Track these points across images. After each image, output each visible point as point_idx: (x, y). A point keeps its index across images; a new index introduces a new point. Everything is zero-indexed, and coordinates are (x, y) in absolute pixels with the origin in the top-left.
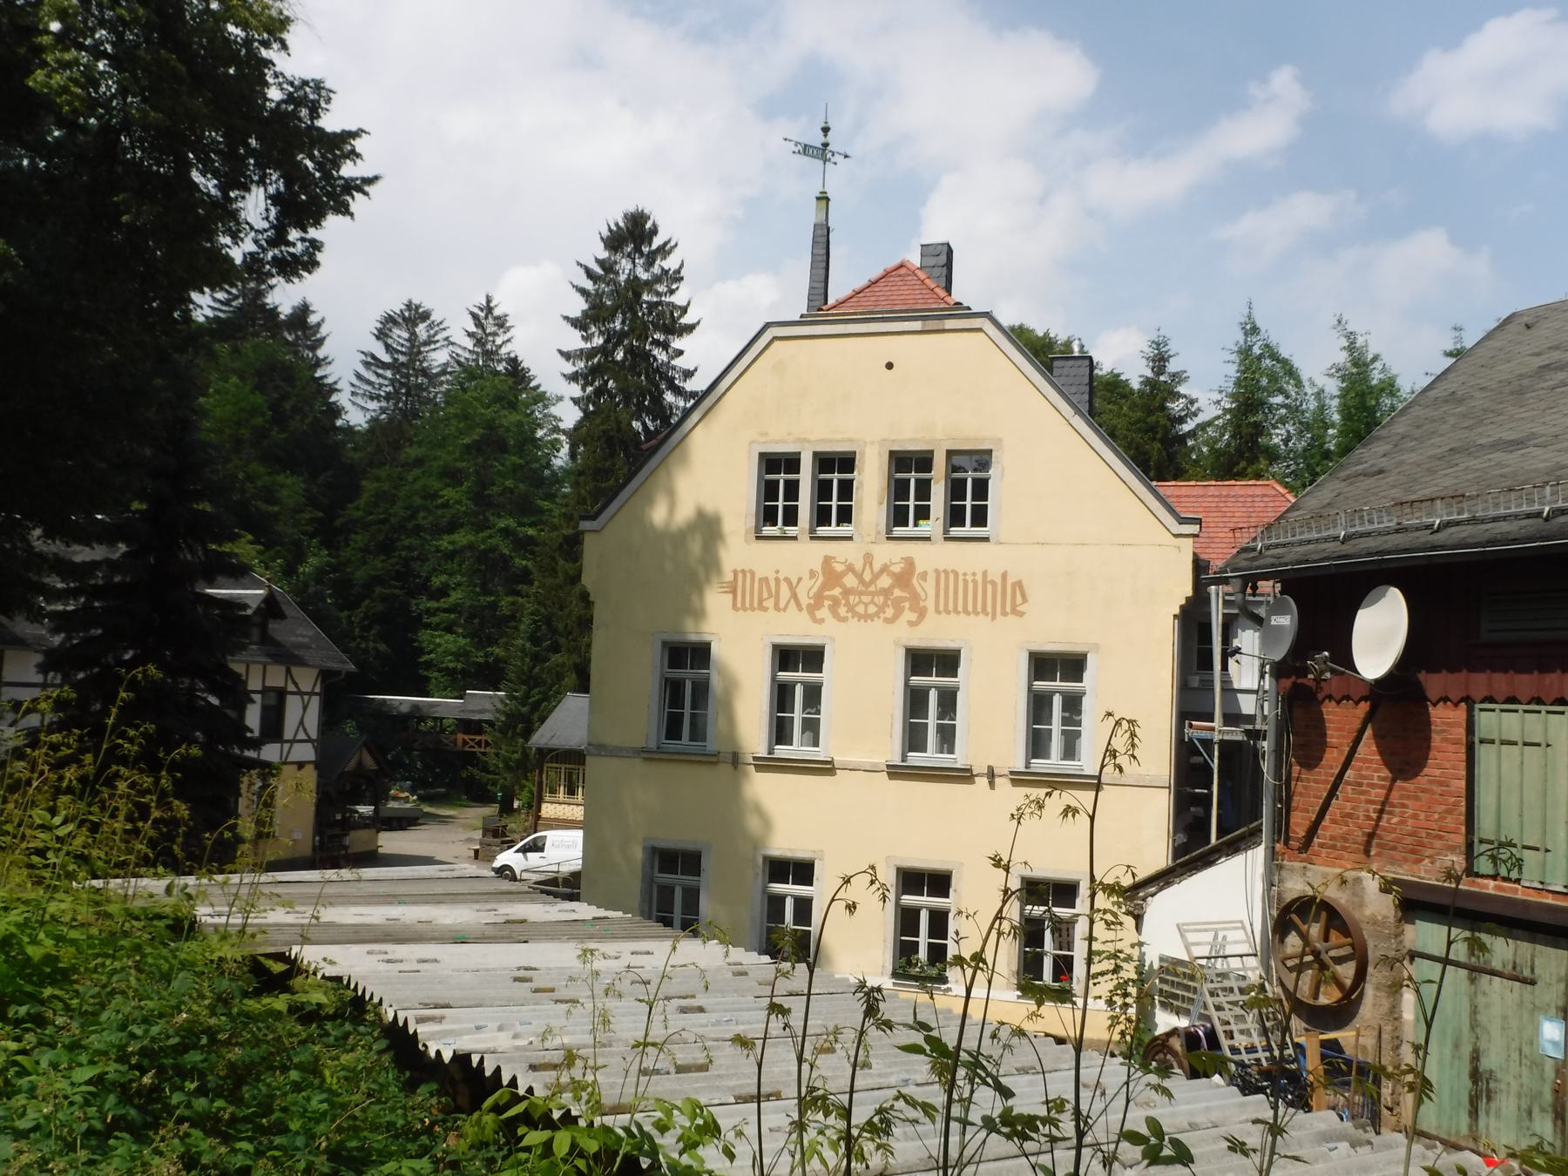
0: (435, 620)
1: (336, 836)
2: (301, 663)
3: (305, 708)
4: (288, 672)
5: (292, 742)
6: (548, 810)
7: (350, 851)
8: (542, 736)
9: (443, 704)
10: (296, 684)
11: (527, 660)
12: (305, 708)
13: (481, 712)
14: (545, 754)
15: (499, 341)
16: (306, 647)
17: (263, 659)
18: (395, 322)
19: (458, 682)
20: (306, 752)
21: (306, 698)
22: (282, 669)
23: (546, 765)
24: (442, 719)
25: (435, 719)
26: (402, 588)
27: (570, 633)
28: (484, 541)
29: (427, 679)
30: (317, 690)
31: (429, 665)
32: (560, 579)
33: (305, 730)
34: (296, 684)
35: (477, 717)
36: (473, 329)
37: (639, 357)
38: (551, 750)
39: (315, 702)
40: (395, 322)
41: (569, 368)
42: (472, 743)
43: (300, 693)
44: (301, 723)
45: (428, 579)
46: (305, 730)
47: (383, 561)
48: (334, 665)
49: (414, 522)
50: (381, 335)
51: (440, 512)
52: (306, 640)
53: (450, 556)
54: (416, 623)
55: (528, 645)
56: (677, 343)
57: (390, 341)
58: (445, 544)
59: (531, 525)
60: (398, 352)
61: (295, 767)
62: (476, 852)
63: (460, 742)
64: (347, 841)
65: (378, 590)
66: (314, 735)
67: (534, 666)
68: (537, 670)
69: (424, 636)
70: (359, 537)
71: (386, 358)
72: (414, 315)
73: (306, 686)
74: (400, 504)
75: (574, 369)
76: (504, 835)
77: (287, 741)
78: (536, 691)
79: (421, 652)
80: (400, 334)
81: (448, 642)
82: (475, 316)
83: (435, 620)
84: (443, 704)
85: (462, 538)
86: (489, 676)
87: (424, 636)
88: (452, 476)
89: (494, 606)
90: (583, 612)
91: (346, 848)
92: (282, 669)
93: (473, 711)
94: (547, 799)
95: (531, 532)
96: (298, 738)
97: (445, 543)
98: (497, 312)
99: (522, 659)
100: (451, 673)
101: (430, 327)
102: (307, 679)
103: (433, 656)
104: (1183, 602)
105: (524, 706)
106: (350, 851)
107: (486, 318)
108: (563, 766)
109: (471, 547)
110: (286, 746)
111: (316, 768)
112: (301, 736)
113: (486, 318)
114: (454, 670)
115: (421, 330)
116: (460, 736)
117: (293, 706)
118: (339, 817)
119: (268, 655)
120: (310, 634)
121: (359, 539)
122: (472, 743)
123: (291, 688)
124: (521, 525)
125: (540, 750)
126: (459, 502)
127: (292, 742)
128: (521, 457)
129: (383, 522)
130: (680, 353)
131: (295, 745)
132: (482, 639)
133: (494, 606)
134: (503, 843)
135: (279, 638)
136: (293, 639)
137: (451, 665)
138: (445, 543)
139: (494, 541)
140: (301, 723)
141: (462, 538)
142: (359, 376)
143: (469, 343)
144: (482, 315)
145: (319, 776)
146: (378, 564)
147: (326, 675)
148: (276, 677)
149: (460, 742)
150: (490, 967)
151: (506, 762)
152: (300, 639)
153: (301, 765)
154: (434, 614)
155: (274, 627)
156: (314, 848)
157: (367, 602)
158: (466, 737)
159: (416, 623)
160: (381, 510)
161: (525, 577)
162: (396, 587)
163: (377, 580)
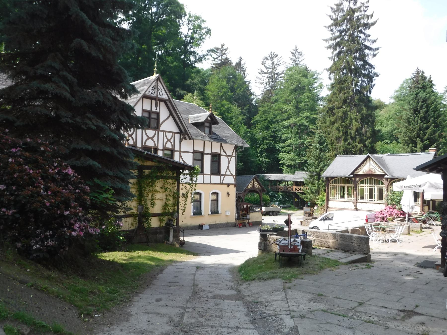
0: (284, 150)
1: (245, 214)
2: (226, 142)
3: (229, 162)
4: (221, 146)
5: (225, 175)
6: (331, 204)
7: (250, 221)
8: (328, 172)
9: (289, 177)
10: (225, 152)
11: (318, 151)
12: (229, 162)
13: (301, 178)
14: (329, 180)
15: (300, 60)
16: (229, 137)
17: (210, 140)
18: (267, 59)
19: (293, 168)
20: (231, 180)
21: (229, 158)
22: (219, 144)
23: (330, 185)
24: (288, 181)
25: (286, 181)
26: (273, 140)
27: (333, 143)
28: (299, 121)
29: (282, 169)
30: (234, 155)
31: (282, 164)
32: (328, 124)
33: (230, 171)
34: (225, 152)
35: (299, 180)
36: (292, 57)
37: (354, 39)
38: (332, 178)
39: (233, 160)
40: (267, 59)
41: (327, 44)
42: (298, 189)
43: (226, 155)
44: (228, 168)
45: (281, 137)
46: (230, 171)
47: (266, 132)
48: (240, 144)
49: (276, 119)
50: (263, 63)
51: (284, 114)
52: (229, 135)
53: (287, 127)
54: (278, 151)
55: (318, 145)
56: (368, 32)
57: (266, 65)
58: (286, 123)
59: (315, 114)
60: (268, 68)
61: (226, 186)
62: (302, 222)
63: (294, 189)
64: (249, 216)
65: (265, 141)
66: (234, 173)
67: (321, 153)
68: (322, 154)
69: (281, 155)
70: (259, 126)
71: (266, 71)
72: (273, 56)
73: (229, 153)
74: (271, 114)
75: (329, 45)
76: (313, 215)
77: (222, 175)
78: (322, 162)
79: (280, 160)
80: (268, 63)
81: (288, 156)
82: (292, 53)
83: (284, 150)
84: (289, 177)
85: (292, 121)
86: (301, 167)
87: (281, 155)
88: (287, 102)
89: (303, 143)
90: (337, 135)
91: (249, 219)
92: (219, 144)
93: (298, 178)
94: (331, 199)
95: (315, 116)
96: (227, 174)
97: (286, 123)
98: (299, 51)
99: (316, 151)
100: (289, 166)
101: (278, 59)
102: (229, 149)
103: (284, 161)
104: (251, 257)
105: (317, 169)
106: (250, 221)
107: (296, 53)
108: (338, 185)
109: (295, 124)
110: (222, 177)
111: (235, 187)
112: (228, 173)
113: (296, 53)
114: (291, 165)
115: (276, 61)
116: (294, 187)
117: (224, 161)
118: (245, 206)
119: (211, 138)
120: (231, 133)
121: (259, 126)
122: (298, 189)
123: (223, 153)
124: (312, 114)
125: (327, 178)
126: (290, 109)
127: (225, 175)
128: (310, 93)
129: (266, 120)
130: (369, 36)
131: (226, 177)
132: (299, 155)
133: (303, 143)
134: (312, 218)
135: (217, 133)
136: (223, 134)
137: (289, 164)
138: (286, 123)
139: (303, 121)
140: (228, 168)
141: (292, 121)
142: (257, 78)
143: (291, 62)
144: (294, 52)
145: (237, 190)
146: (265, 133)
147: (237, 148)
148: (216, 149)
149: (294, 189)
150: (349, 329)
151: (311, 190)
152: (226, 134)
153: (229, 185)
154: (284, 147)
155: (215, 128)
156: (236, 219)
157: (262, 145)
158: (296, 187)
159: (278, 151)
160: (265, 116)
161: (314, 133)
162: (271, 140)
163: (264, 138)
